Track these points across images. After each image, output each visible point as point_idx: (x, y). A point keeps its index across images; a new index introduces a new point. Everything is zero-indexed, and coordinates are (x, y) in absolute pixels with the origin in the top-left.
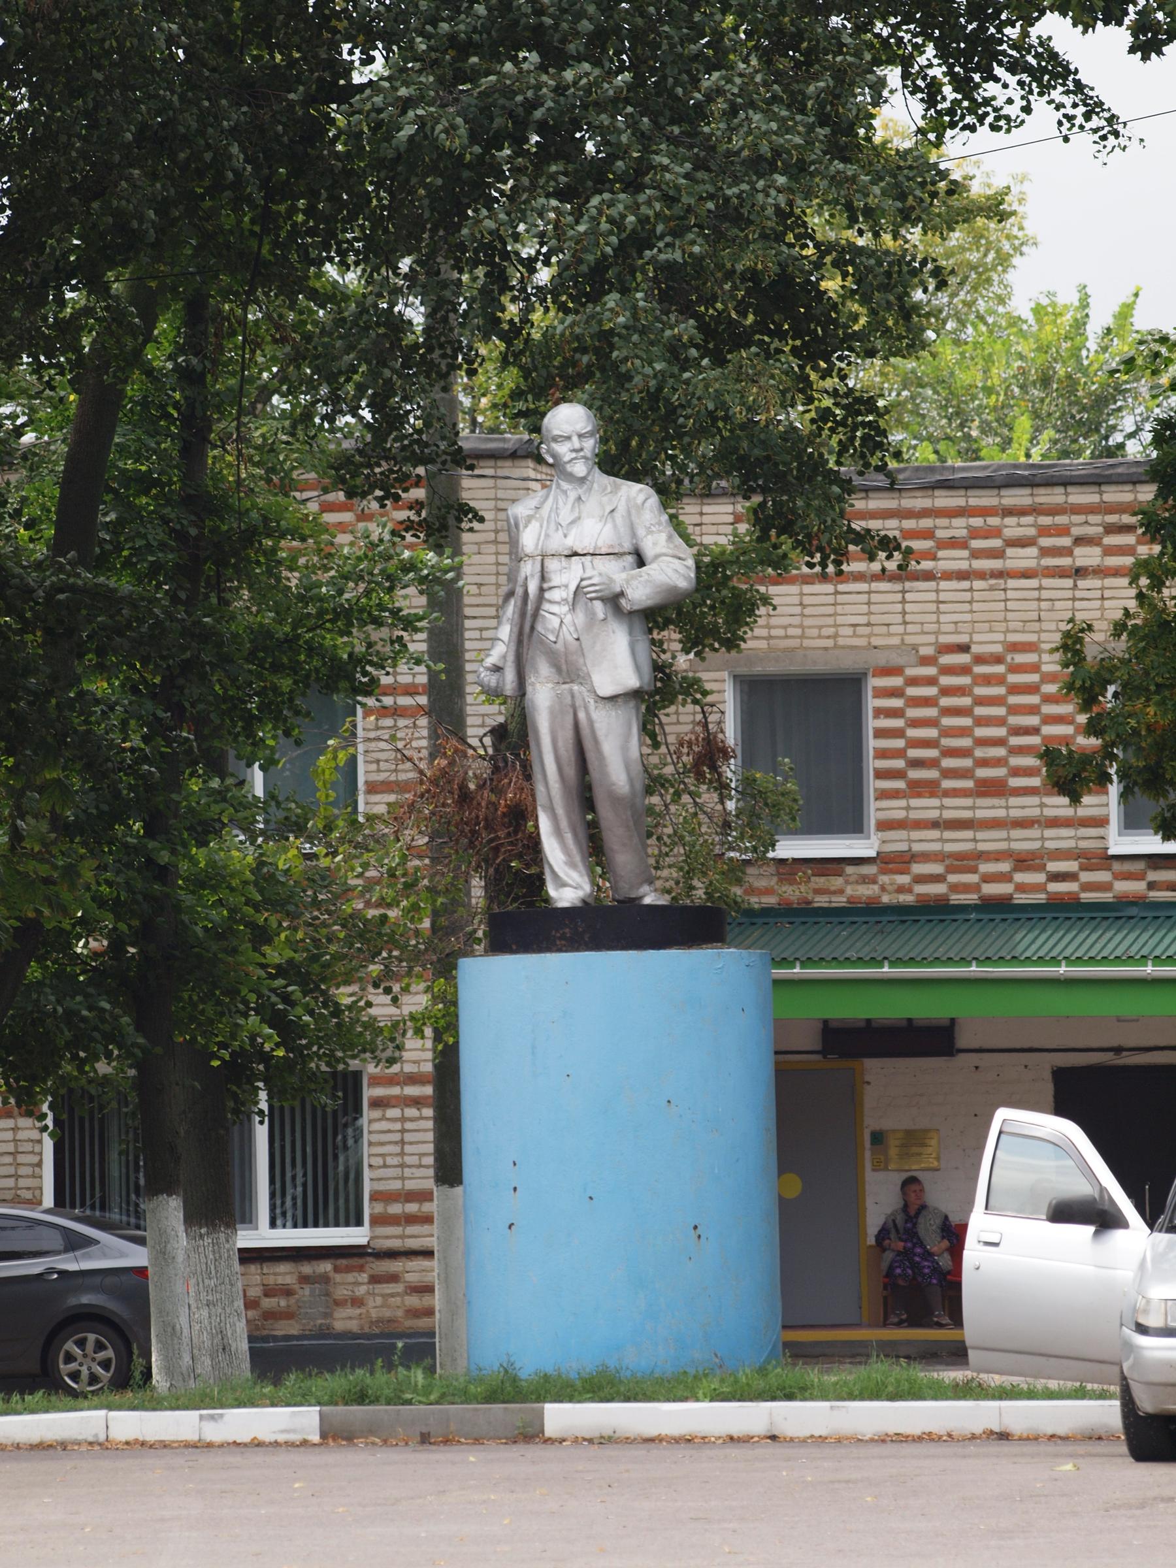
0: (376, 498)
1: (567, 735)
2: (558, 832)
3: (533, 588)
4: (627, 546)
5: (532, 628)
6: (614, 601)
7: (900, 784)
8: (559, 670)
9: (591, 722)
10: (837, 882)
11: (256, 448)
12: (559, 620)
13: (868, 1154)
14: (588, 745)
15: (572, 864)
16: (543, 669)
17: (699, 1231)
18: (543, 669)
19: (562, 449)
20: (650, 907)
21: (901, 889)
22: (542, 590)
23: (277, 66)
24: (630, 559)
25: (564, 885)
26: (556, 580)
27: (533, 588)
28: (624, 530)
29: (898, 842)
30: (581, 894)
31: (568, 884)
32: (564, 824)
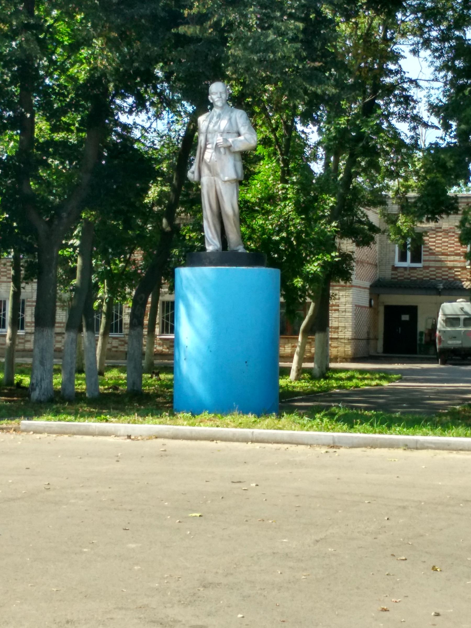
4: (235, 129)
5: (203, 158)
6: (229, 148)
7: (427, 253)
8: (210, 172)
9: (220, 190)
10: (415, 271)
13: (6, 398)
14: (220, 198)
17: (248, 363)
20: (241, 253)
21: (427, 273)
22: (206, 145)
24: (236, 135)
26: (210, 141)
29: (427, 264)
30: (216, 248)
31: (212, 245)
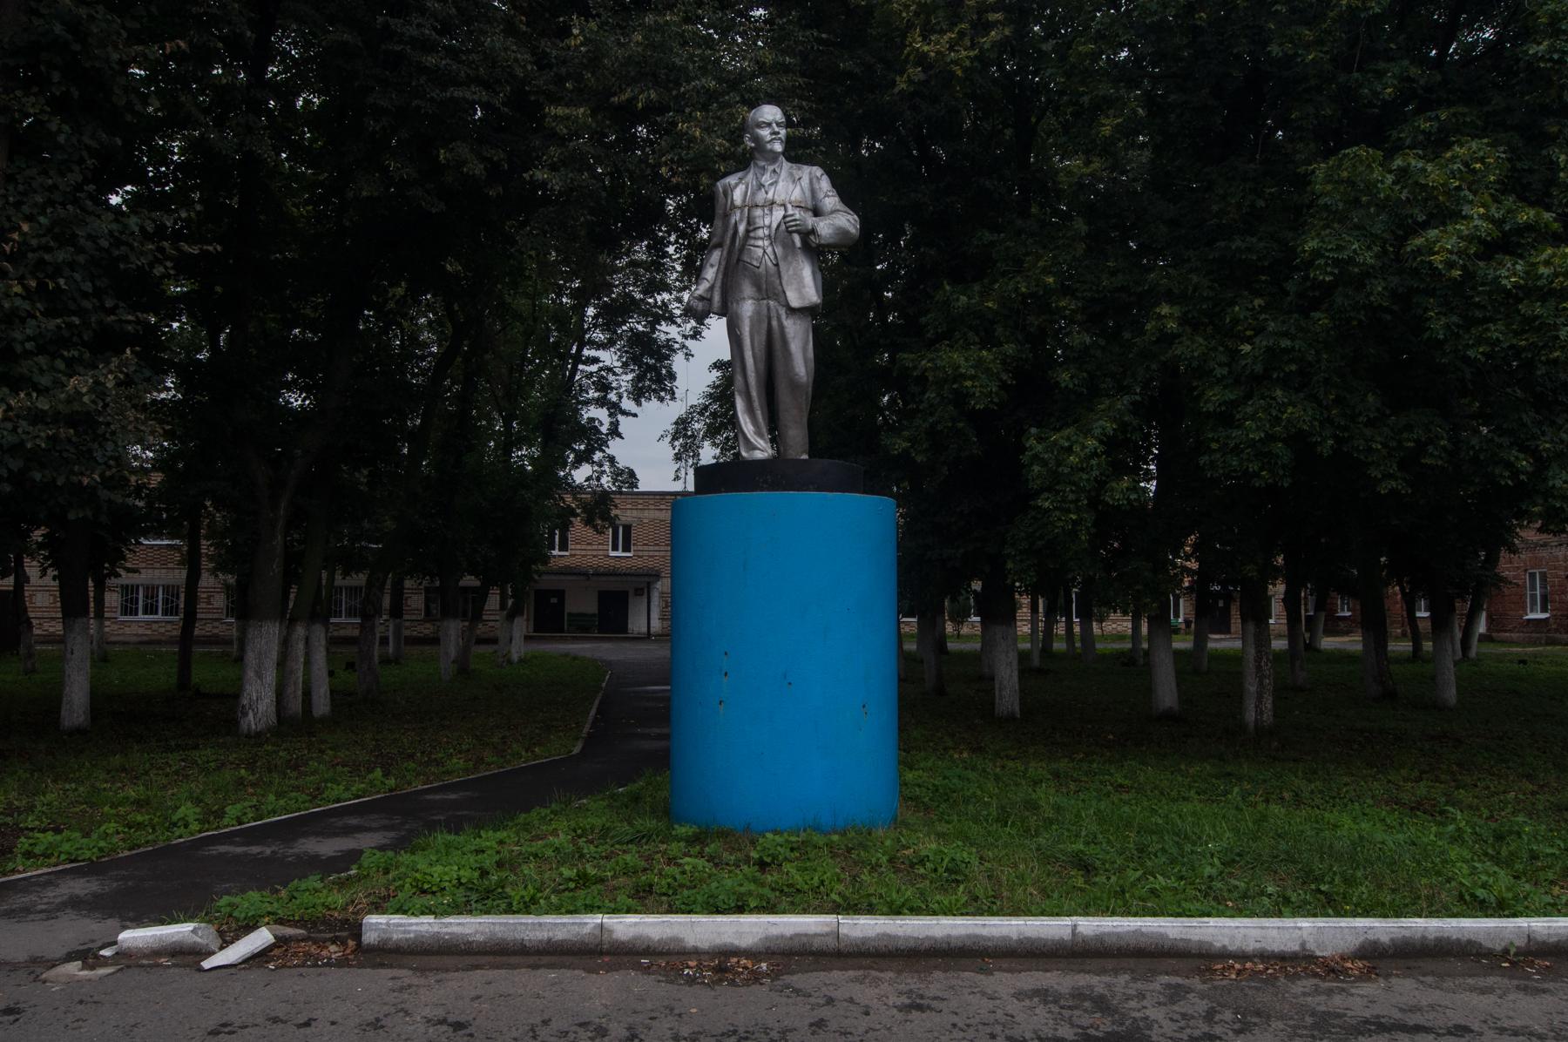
0: (1126, 149)
1: (762, 338)
2: (750, 410)
3: (742, 228)
9: (782, 327)
11: (1397, 253)
12: (762, 251)
15: (759, 434)
16: (748, 289)
18: (748, 289)
19: (765, 133)
22: (747, 231)
23: (825, 130)
25: (755, 448)
27: (742, 228)
28: (808, 193)
32: (756, 404)
